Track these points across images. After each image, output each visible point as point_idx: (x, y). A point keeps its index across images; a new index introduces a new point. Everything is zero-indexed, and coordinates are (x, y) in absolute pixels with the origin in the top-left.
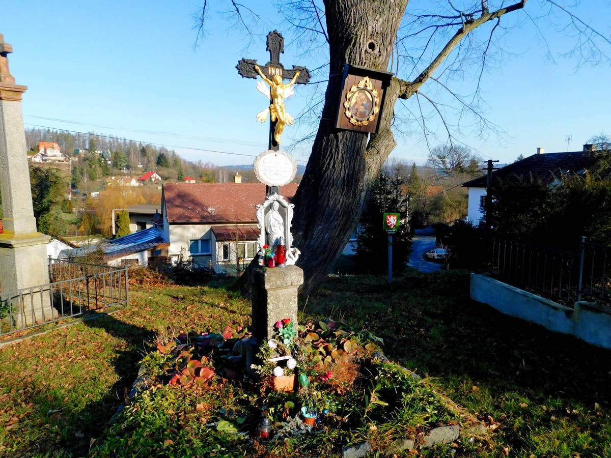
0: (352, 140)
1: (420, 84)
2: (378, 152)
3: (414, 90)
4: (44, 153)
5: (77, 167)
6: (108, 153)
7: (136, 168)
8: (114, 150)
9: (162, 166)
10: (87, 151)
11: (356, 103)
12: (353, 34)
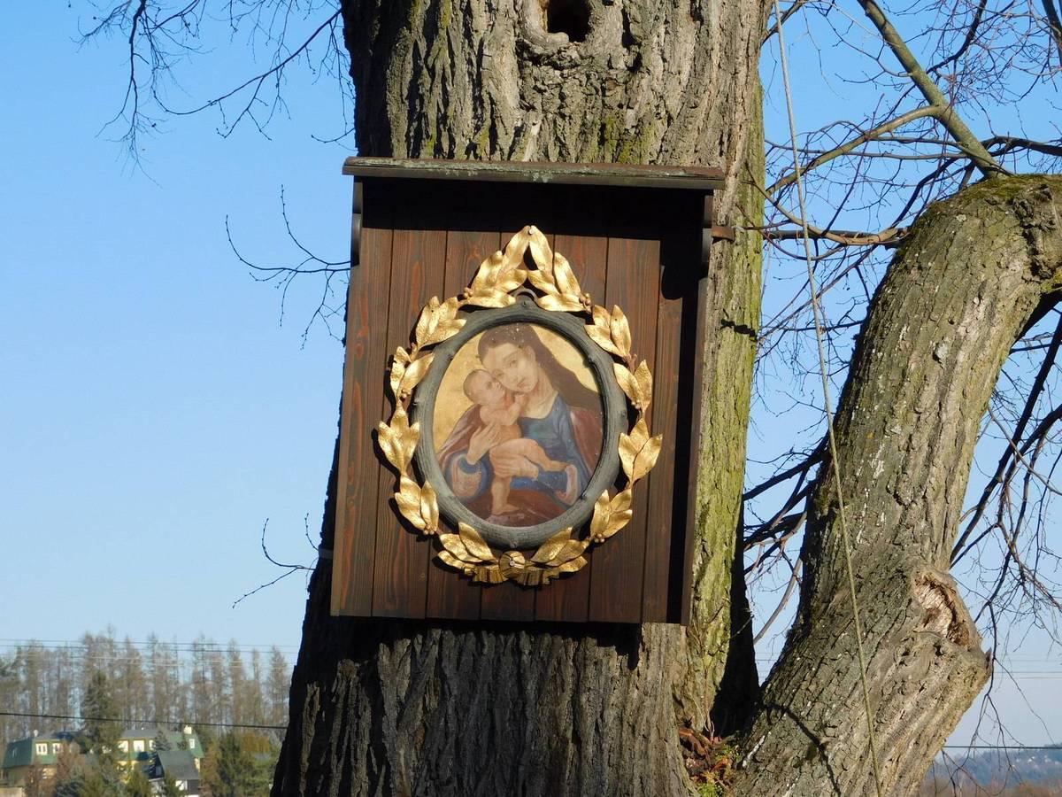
0: (494, 690)
2: (817, 749)
8: (220, 731)
10: (73, 747)
11: (473, 420)
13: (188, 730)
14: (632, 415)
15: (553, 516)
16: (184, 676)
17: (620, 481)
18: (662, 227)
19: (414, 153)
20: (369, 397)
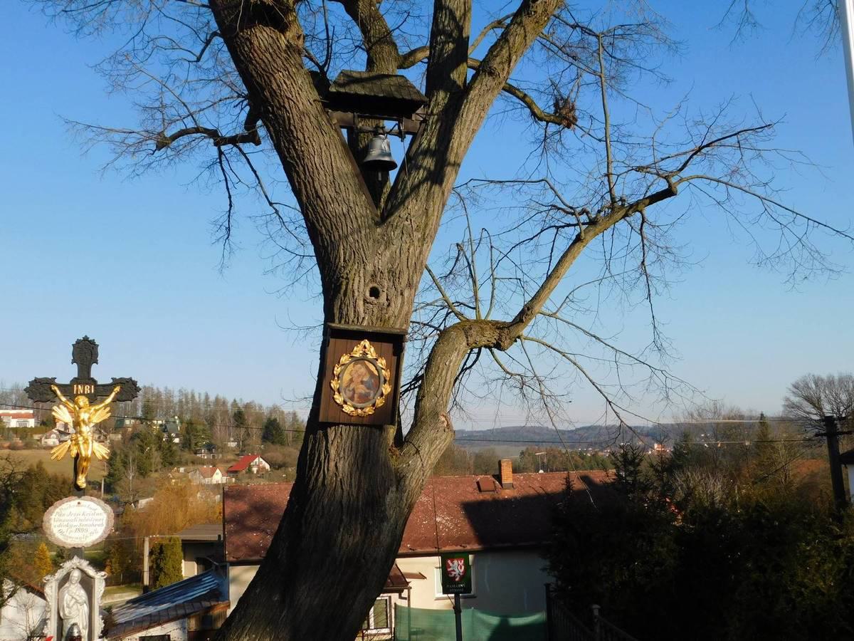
1: (522, 325)
2: (418, 452)
3: (513, 334)
4: (63, 430)
5: (118, 452)
6: (175, 422)
7: (224, 449)
8: (187, 417)
9: (273, 443)
10: (138, 422)
11: (351, 381)
12: (343, 277)
13: (176, 417)
14: (385, 381)
15: (367, 402)
16: (176, 400)
17: (382, 395)
18: (394, 342)
19: (340, 322)
20: (324, 373)
